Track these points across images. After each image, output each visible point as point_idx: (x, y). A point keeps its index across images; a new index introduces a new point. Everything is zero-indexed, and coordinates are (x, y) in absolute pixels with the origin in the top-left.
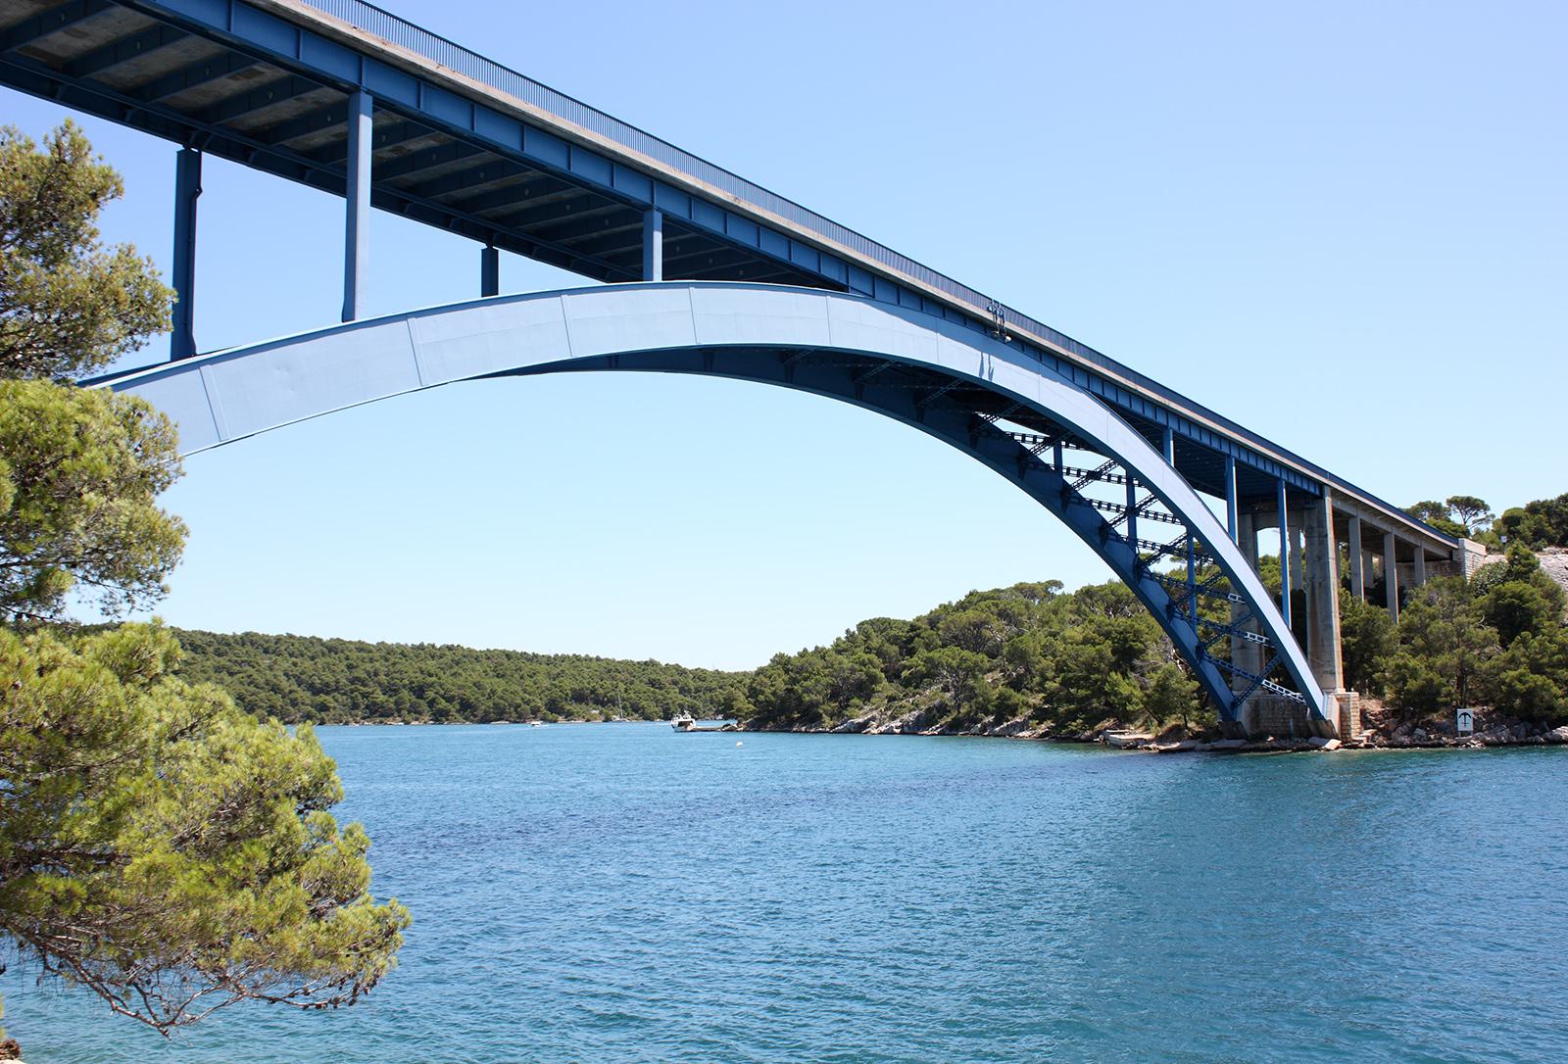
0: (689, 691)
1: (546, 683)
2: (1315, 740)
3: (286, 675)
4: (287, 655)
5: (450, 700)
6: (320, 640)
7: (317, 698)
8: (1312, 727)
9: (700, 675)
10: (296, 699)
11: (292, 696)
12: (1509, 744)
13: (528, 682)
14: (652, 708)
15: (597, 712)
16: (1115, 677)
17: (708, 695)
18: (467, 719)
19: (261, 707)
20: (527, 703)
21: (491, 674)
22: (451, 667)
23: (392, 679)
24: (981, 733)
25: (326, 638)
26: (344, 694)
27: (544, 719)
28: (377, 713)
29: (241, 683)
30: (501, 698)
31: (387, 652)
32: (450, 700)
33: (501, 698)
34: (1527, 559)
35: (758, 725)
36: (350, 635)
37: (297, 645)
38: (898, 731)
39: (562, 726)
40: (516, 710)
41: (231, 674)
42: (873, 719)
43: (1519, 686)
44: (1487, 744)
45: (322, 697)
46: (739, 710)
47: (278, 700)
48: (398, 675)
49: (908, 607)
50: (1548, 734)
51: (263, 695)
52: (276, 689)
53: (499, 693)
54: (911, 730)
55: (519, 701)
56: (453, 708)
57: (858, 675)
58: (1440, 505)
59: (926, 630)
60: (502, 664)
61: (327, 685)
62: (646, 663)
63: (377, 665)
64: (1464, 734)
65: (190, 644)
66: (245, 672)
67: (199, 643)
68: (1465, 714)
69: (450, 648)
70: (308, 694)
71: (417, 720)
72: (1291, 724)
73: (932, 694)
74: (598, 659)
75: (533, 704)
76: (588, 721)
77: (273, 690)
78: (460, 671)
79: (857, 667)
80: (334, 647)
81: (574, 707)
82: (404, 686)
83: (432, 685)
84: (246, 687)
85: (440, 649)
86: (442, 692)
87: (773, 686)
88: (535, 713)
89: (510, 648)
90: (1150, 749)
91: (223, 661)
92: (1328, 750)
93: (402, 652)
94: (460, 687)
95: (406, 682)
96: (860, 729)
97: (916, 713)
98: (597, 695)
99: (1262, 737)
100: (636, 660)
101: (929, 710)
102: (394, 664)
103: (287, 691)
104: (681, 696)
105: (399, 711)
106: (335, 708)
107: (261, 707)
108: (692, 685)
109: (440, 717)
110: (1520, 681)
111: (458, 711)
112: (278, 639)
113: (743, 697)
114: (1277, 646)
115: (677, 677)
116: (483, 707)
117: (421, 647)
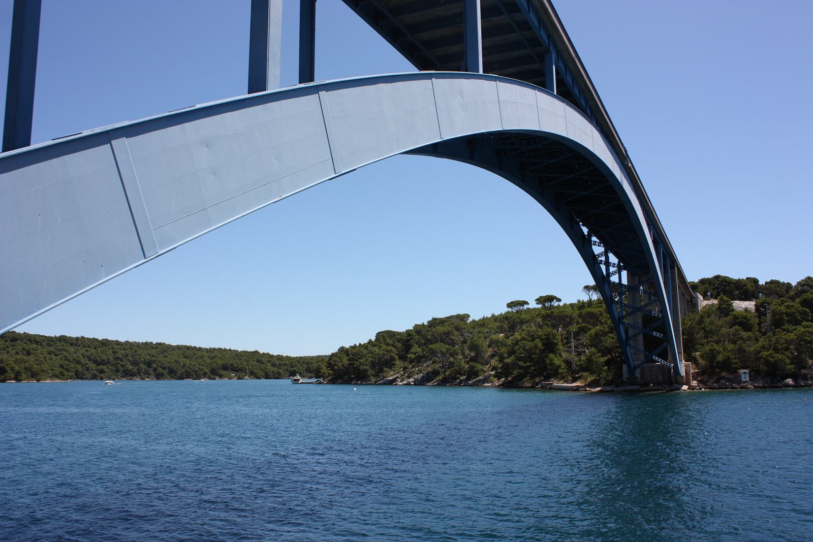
0: (276, 365)
1: (209, 361)
2: (676, 386)
3: (83, 355)
4: (82, 346)
5: (164, 368)
6: (97, 339)
7: (99, 367)
8: (673, 379)
9: (279, 358)
10: (88, 367)
11: (87, 366)
12: (764, 387)
13: (200, 360)
14: (260, 373)
15: (234, 375)
17: (285, 367)
18: (172, 377)
19: (71, 371)
20: (201, 370)
21: (182, 356)
22: (162, 353)
23: (135, 358)
24: (459, 384)
25: (100, 339)
26: (112, 365)
27: (209, 378)
28: (128, 374)
29: (61, 359)
30: (188, 368)
31: (129, 345)
32: (164, 368)
33: (188, 368)
35: (333, 381)
36: (112, 338)
37: (86, 342)
38: (413, 383)
39: (218, 381)
40: (196, 374)
41: (56, 355)
42: (398, 377)
43: (771, 359)
44: (756, 387)
45: (101, 367)
46: (324, 373)
47: (79, 368)
48: (138, 357)
49: (402, 325)
51: (72, 365)
52: (78, 362)
53: (187, 365)
54: (420, 383)
55: (197, 369)
56: (165, 372)
57: (386, 357)
59: (415, 336)
60: (186, 352)
61: (104, 361)
62: (254, 352)
63: (128, 352)
64: (746, 382)
65: (35, 341)
66: (63, 354)
67: (39, 340)
68: (745, 373)
69: (160, 344)
70: (94, 365)
71: (148, 378)
72: (660, 378)
73: (427, 367)
74: (230, 350)
75: (204, 371)
76: (230, 379)
77: (77, 363)
78: (167, 355)
79: (385, 353)
80: (105, 343)
81: (223, 372)
82: (141, 361)
83: (155, 361)
84: (64, 361)
85: (155, 345)
86: (160, 365)
87: (341, 362)
88: (205, 375)
89: (188, 345)
90: (587, 391)
91: (52, 349)
92: (685, 390)
93: (138, 345)
94: (169, 362)
95: (142, 360)
96: (391, 383)
97: (421, 375)
98: (233, 367)
99: (647, 384)
100: (249, 350)
101: (428, 373)
102: (136, 351)
103: (84, 363)
104: (272, 368)
105: (139, 373)
106: (107, 372)
107: (71, 371)
108: (277, 363)
109: (159, 376)
110: (771, 357)
111: (168, 374)
112: (77, 339)
113: (324, 368)
114: (650, 340)
115: (270, 359)
116: (180, 372)
117: (146, 343)
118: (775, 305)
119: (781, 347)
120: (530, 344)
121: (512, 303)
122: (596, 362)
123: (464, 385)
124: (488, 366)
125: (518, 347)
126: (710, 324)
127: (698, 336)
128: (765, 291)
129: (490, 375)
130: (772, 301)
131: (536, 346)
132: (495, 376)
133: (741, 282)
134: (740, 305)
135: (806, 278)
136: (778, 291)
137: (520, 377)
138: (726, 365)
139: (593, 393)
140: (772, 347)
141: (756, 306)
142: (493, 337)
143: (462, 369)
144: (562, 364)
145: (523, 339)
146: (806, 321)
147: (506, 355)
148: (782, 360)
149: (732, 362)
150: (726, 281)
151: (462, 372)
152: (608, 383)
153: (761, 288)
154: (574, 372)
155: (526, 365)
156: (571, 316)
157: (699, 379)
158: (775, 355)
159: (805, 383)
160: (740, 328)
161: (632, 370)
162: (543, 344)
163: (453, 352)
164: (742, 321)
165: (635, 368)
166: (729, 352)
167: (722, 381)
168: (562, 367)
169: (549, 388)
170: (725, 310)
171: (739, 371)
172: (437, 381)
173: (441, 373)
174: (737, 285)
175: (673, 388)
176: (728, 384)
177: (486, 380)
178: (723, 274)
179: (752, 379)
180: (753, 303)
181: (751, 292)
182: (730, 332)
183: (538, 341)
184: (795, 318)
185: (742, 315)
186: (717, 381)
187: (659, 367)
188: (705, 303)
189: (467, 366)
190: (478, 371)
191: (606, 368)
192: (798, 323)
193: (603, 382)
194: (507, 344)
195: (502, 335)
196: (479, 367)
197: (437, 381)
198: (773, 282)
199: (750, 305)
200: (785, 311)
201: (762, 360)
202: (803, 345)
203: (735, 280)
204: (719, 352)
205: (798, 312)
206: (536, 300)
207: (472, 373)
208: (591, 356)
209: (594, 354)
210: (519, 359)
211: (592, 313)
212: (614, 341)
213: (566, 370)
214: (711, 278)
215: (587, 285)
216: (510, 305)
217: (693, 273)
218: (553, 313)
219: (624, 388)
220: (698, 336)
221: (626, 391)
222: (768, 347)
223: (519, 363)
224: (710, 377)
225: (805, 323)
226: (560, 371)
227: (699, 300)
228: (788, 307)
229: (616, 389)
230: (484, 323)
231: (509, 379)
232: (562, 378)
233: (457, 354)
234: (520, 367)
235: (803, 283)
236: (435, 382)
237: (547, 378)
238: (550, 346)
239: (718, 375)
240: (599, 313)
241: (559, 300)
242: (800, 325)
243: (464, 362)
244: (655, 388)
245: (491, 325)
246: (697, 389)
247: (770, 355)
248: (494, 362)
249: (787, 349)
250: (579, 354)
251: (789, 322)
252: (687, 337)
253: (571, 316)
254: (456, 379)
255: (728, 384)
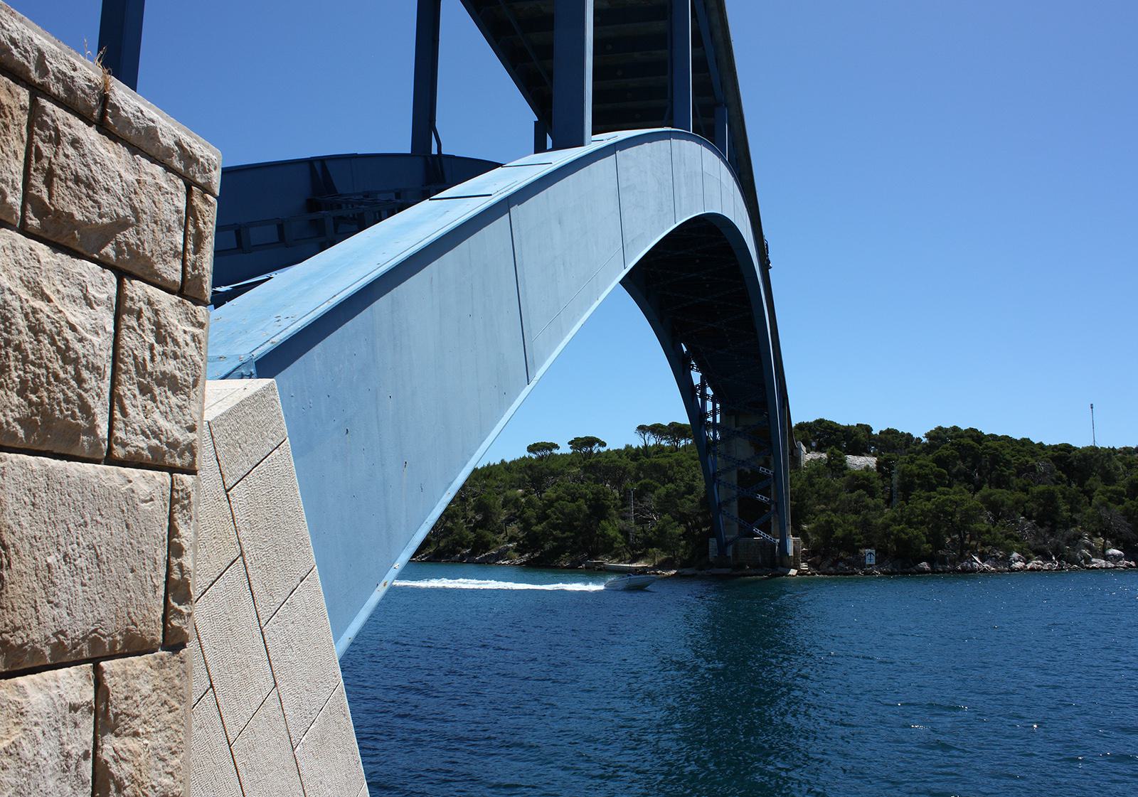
2: (781, 569)
8: (778, 561)
12: (892, 573)
16: (604, 524)
24: (461, 561)
34: (840, 457)
43: (903, 536)
44: (884, 573)
50: (916, 567)
56: (197, 325)
58: (524, 457)
64: (871, 566)
68: (870, 553)
72: (760, 558)
90: (658, 574)
92: (793, 576)
99: (741, 566)
118: (901, 463)
119: (916, 520)
120: (571, 506)
121: (535, 445)
122: (670, 534)
123: (467, 562)
124: (502, 535)
125: (553, 509)
126: (827, 486)
127: (810, 502)
128: (879, 444)
129: (508, 549)
130: (898, 457)
131: (579, 509)
132: (516, 551)
133: (851, 430)
134: (857, 462)
135: (936, 429)
136: (896, 444)
137: (556, 553)
138: (849, 545)
139: (668, 577)
140: (905, 519)
141: (878, 463)
142: (510, 493)
143: (464, 539)
144: (619, 535)
145: (559, 498)
146: (942, 486)
147: (533, 521)
148: (917, 537)
149: (854, 539)
150: (831, 428)
151: (464, 543)
152: (685, 564)
153: (874, 439)
154: (634, 547)
155: (565, 535)
156: (625, 468)
157: (809, 560)
158: (910, 530)
159: (943, 568)
160: (865, 493)
161: (722, 547)
162: (589, 507)
163: (452, 513)
164: (860, 482)
165: (727, 544)
166: (851, 524)
167: (841, 564)
168: (618, 540)
169: (599, 570)
170: (837, 467)
171: (862, 551)
172: (426, 555)
173: (432, 543)
174: (845, 434)
175: (777, 572)
176: (847, 568)
177: (502, 555)
178: (828, 417)
179: (879, 562)
180: (874, 460)
181: (863, 444)
182: (851, 498)
183: (582, 501)
184: (928, 482)
185: (863, 476)
186: (834, 564)
187: (759, 543)
188: (808, 457)
189: (472, 536)
190: (489, 541)
191: (683, 543)
192: (932, 488)
193: (678, 562)
194: (535, 505)
195: (520, 490)
196: (490, 536)
197: (426, 555)
198: (891, 432)
199: (871, 461)
200: (916, 472)
201: (892, 537)
202: (942, 518)
203: (843, 426)
204: (838, 525)
205: (933, 473)
206: (569, 443)
207: (481, 545)
208: (664, 526)
209: (669, 523)
210: (555, 527)
211: (659, 465)
212: (695, 504)
213: (624, 544)
214: (811, 423)
215: (642, 424)
216: (531, 449)
217: (801, 412)
218: (599, 462)
219: (710, 571)
220: (810, 502)
221: (713, 575)
222: (899, 519)
223: (554, 533)
224: (824, 557)
225: (940, 489)
226: (616, 545)
227: (802, 453)
228: (921, 466)
229: (699, 573)
230: (490, 474)
231: (537, 555)
232: (617, 556)
233: (457, 516)
234: (556, 539)
235: (933, 434)
236: (423, 557)
237: (593, 555)
238: (599, 509)
239: (835, 557)
240: (668, 465)
241: (603, 444)
242: (935, 490)
243: (466, 528)
244: (753, 571)
245: (504, 476)
246: (808, 575)
247: (902, 531)
248: (514, 528)
249: (922, 523)
250: (641, 522)
251: (921, 486)
252: (795, 503)
253: (625, 468)
254: (455, 553)
255: (847, 568)
